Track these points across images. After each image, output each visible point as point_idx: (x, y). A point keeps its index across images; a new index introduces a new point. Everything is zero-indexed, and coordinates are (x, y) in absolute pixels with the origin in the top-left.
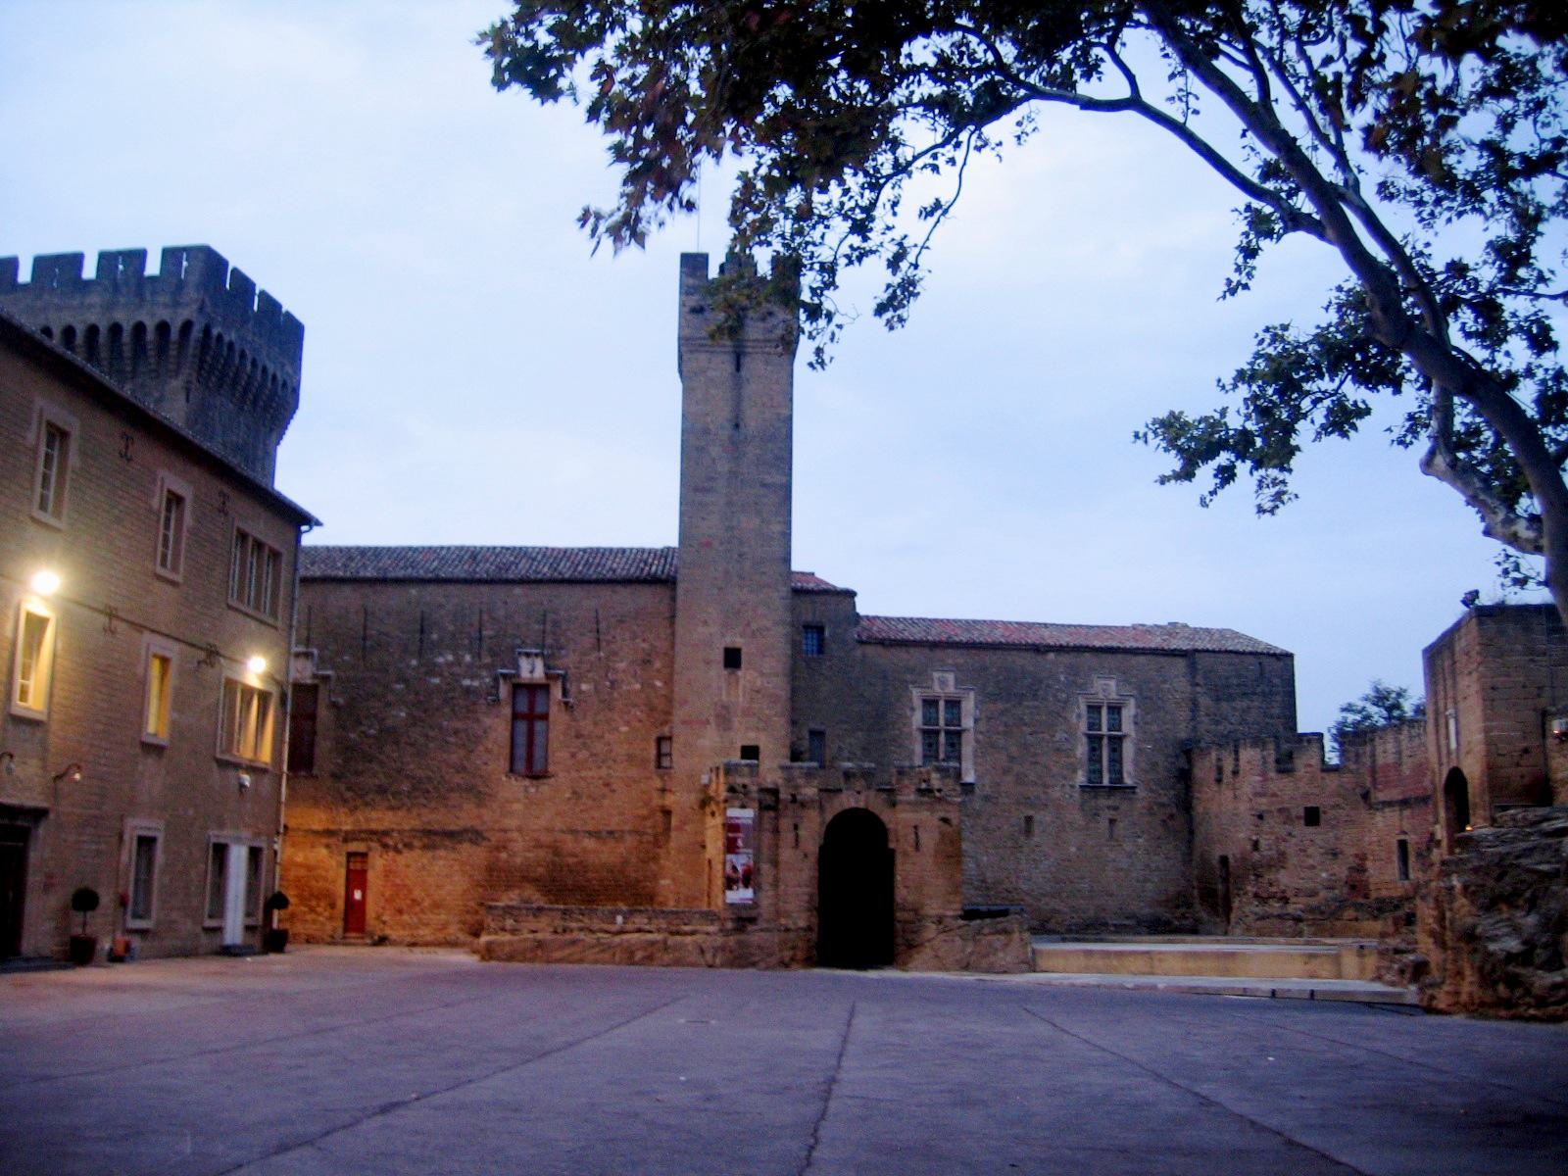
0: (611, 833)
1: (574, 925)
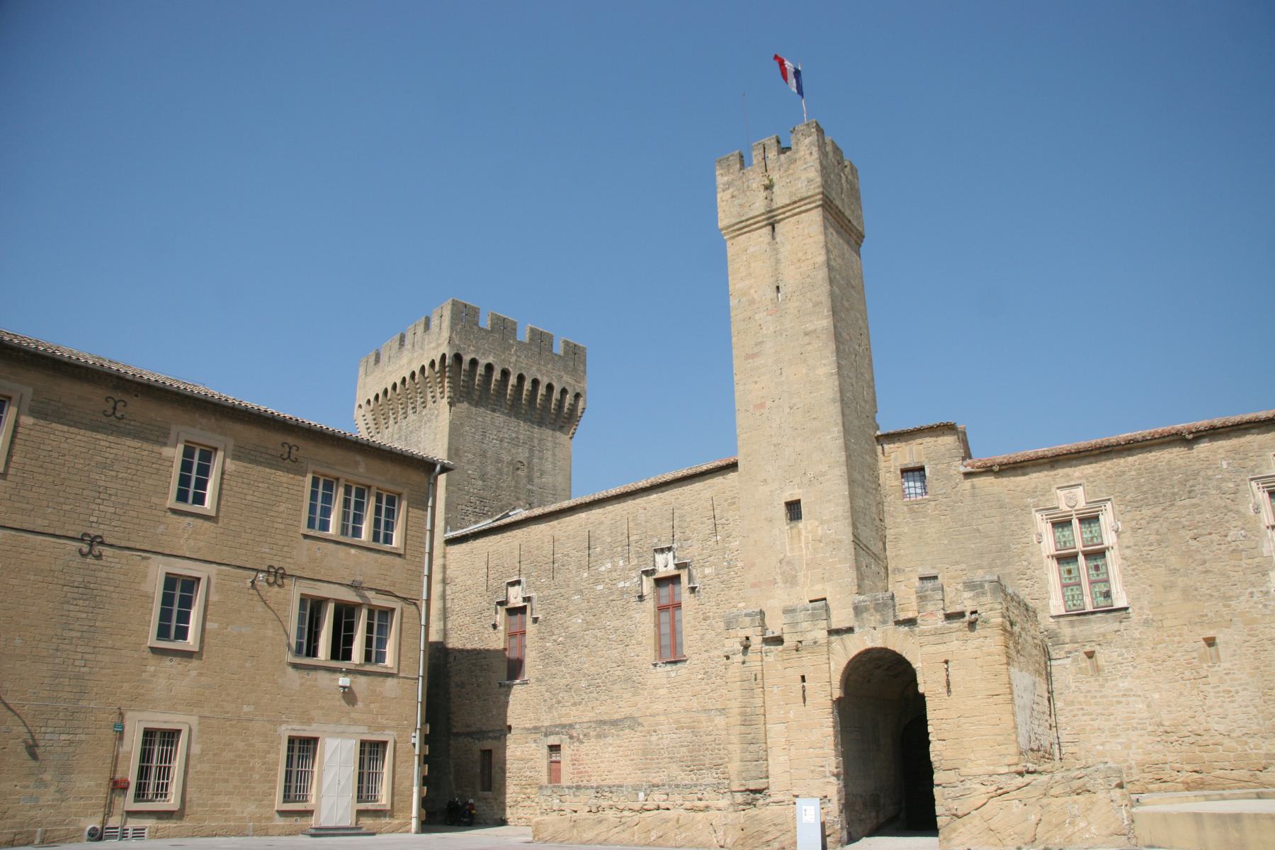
1: (605, 803)
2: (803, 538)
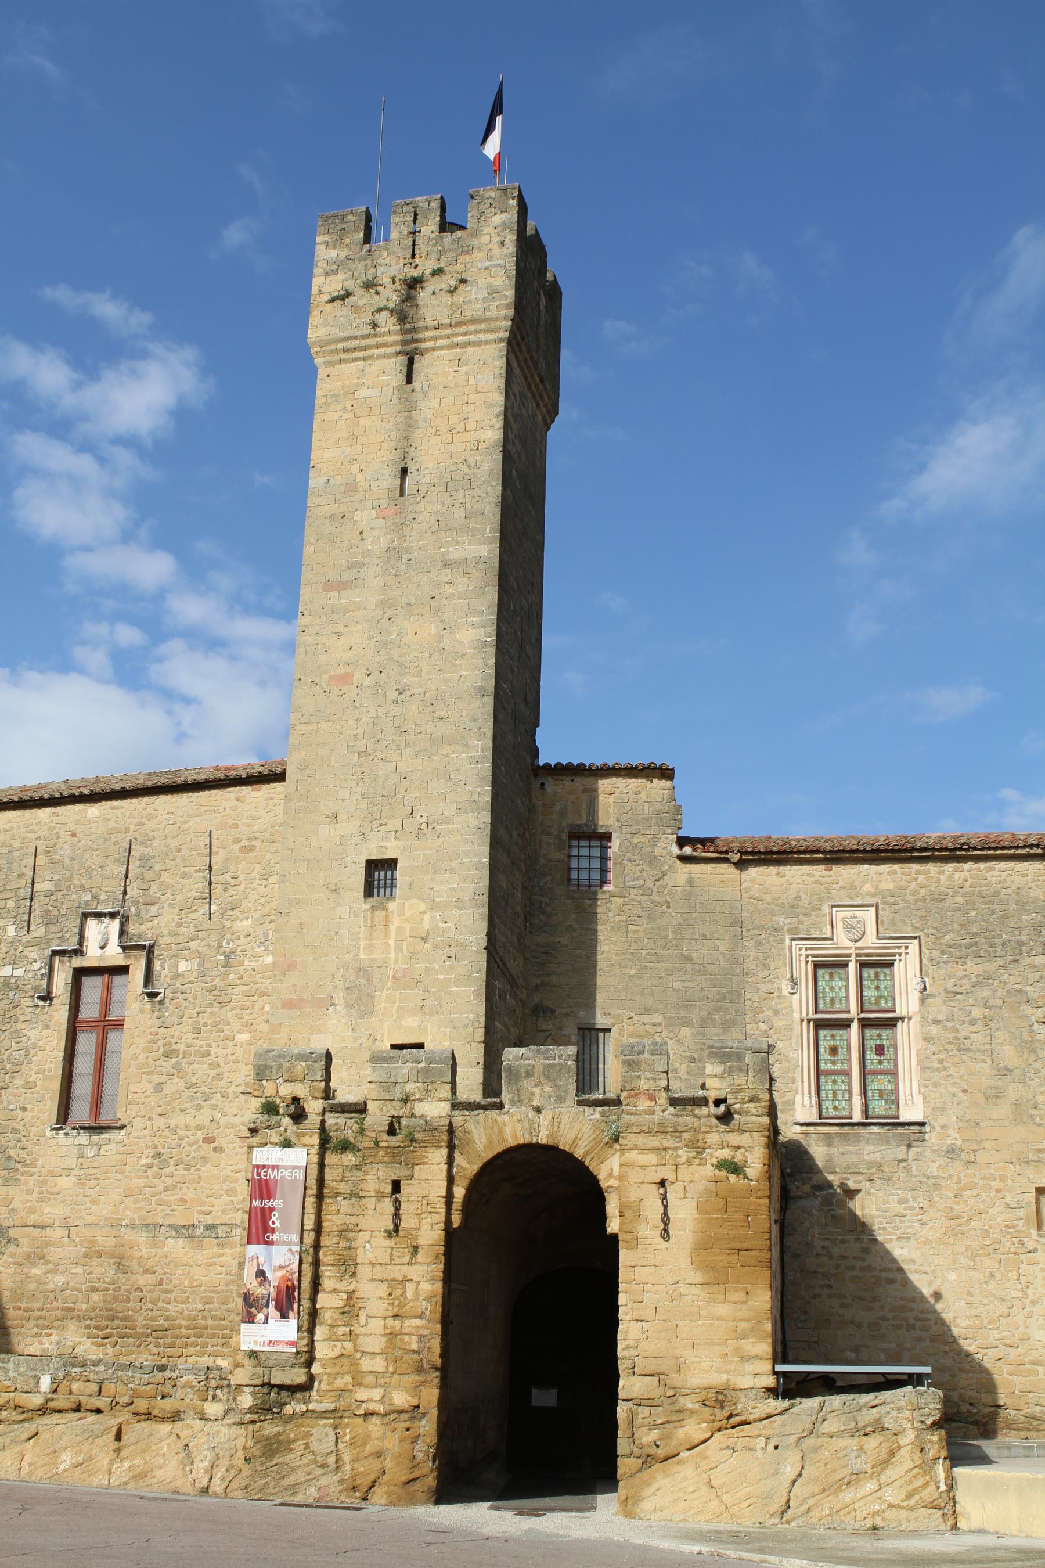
0: (211, 1227)
2: (393, 929)
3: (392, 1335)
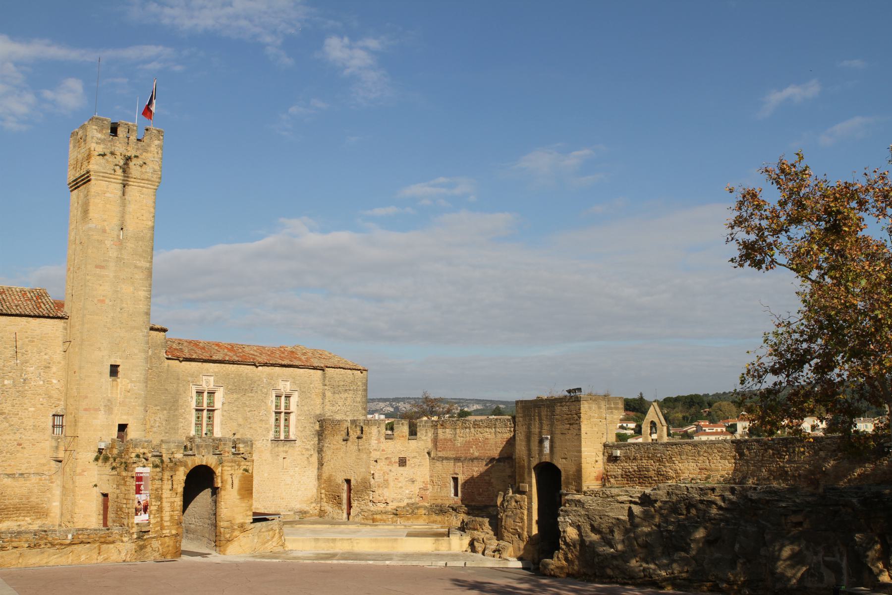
0: (22, 474)
3: (171, 516)
